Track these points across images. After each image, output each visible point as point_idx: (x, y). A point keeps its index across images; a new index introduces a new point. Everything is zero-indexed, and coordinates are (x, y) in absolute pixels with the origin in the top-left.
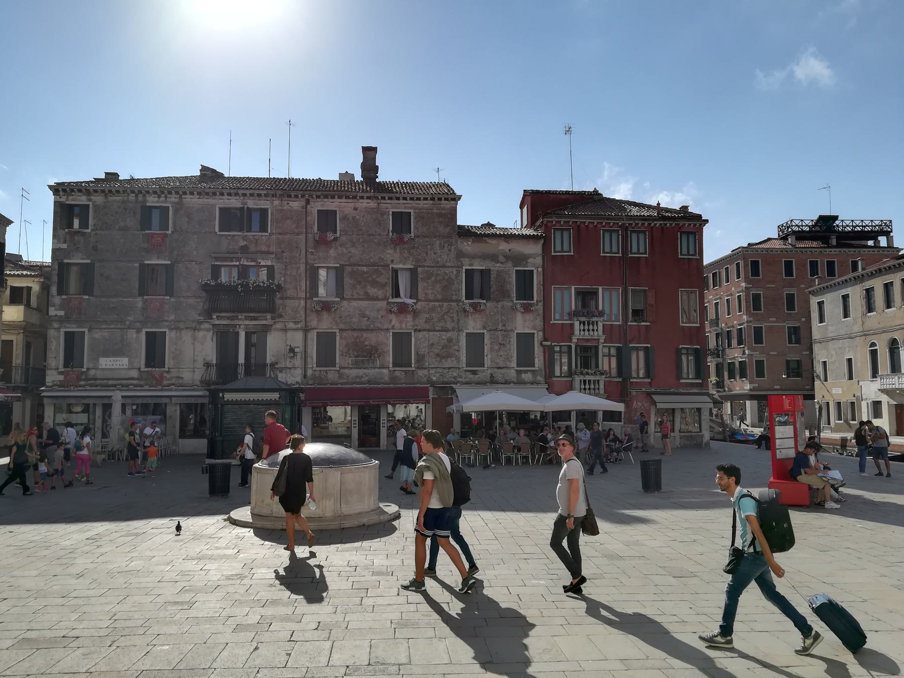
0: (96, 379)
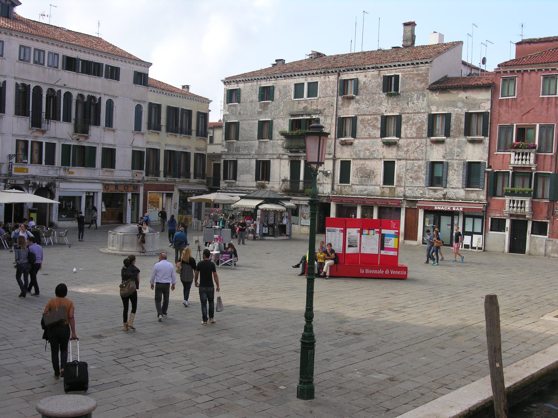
0: (239, 187)
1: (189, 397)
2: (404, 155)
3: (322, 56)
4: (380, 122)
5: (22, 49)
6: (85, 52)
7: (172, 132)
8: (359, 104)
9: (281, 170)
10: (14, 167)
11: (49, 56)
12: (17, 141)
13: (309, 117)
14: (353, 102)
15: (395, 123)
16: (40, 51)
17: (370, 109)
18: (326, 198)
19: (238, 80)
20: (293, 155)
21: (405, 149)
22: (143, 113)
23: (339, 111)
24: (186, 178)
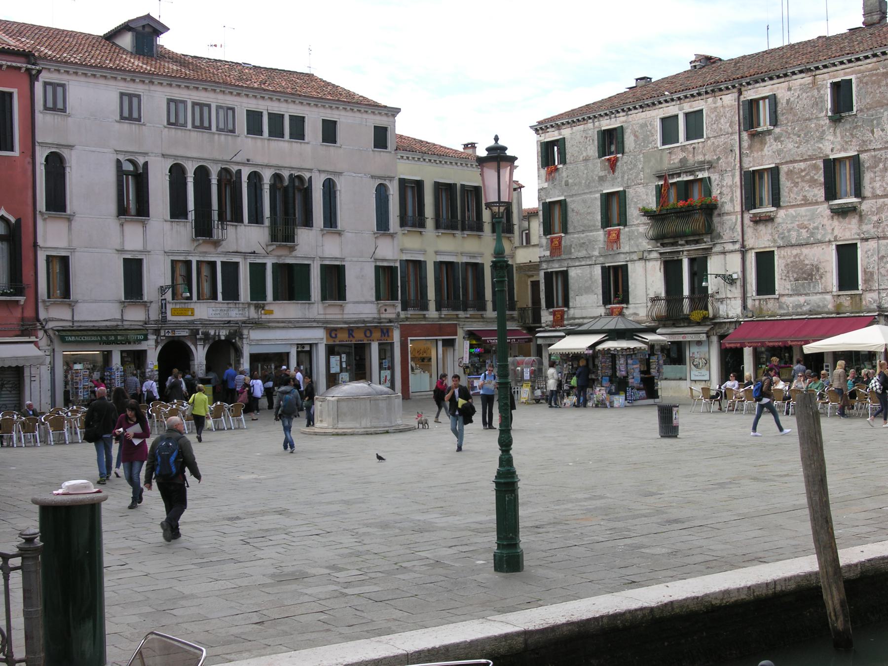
0: (574, 318)
1: (328, 571)
2: (872, 231)
3: (714, 62)
4: (822, 171)
5: (172, 105)
6: (279, 100)
7: (447, 228)
8: (781, 142)
9: (647, 281)
10: (169, 307)
11: (217, 113)
12: (174, 263)
13: (691, 178)
14: (769, 139)
15: (852, 172)
16: (201, 105)
17: (802, 149)
18: (733, 326)
19: (559, 122)
20: (668, 249)
21: (875, 218)
22: (391, 198)
23: (745, 159)
24: (478, 310)
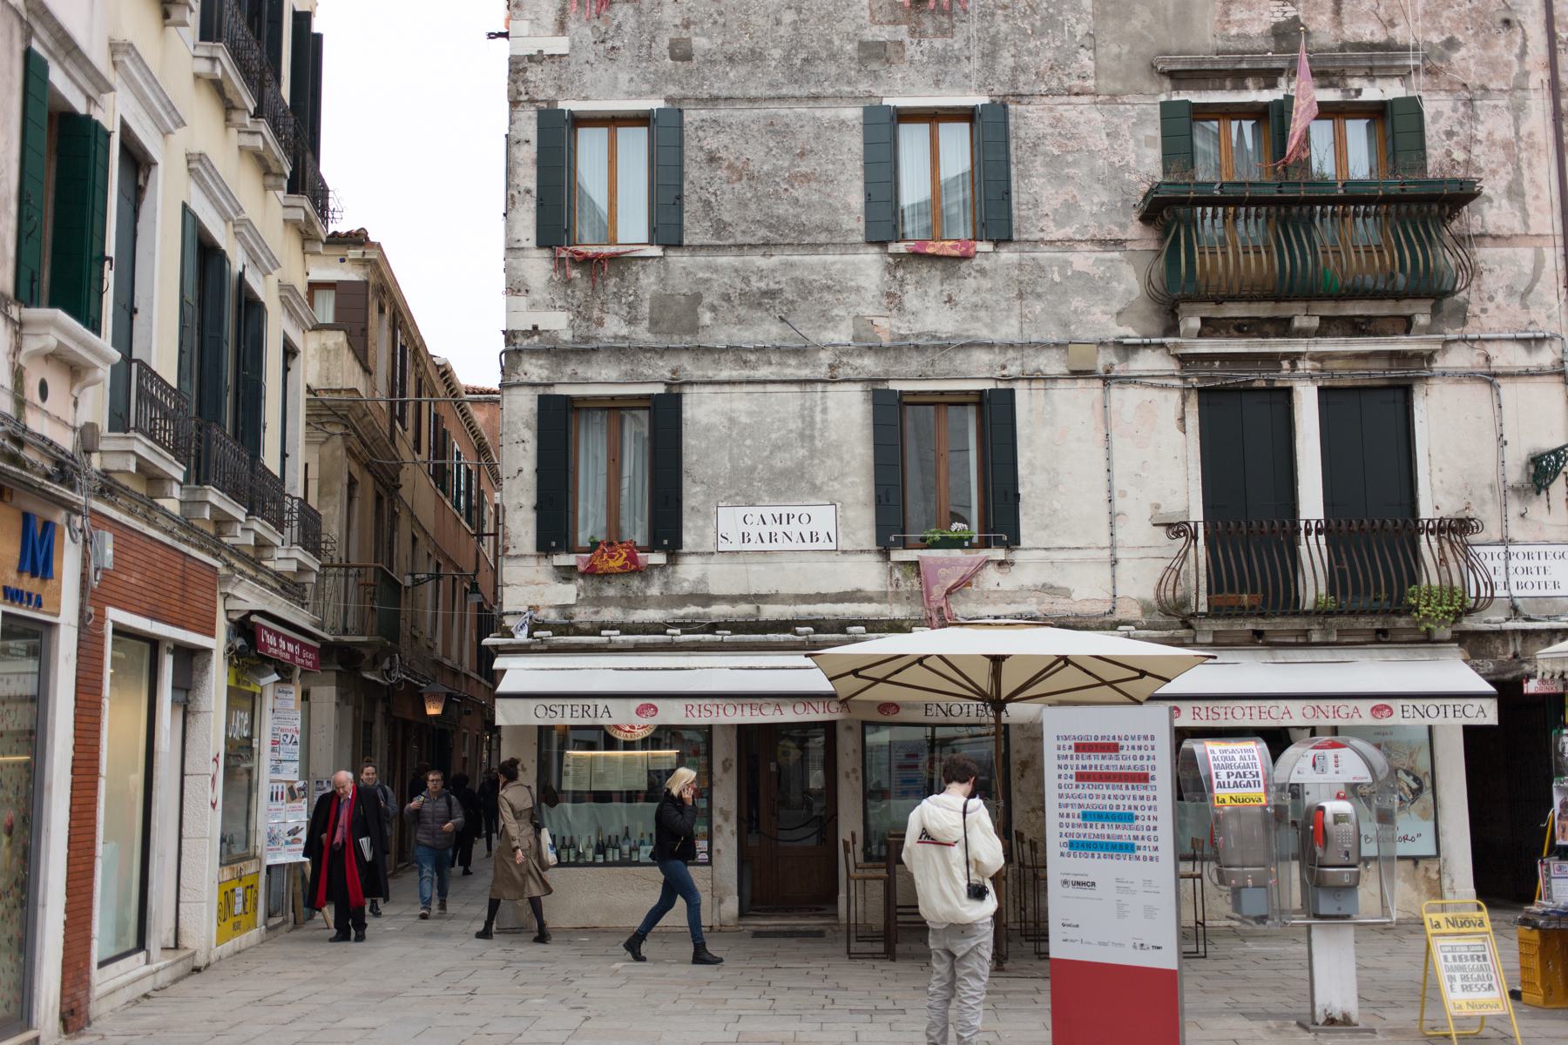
0: (708, 599)
